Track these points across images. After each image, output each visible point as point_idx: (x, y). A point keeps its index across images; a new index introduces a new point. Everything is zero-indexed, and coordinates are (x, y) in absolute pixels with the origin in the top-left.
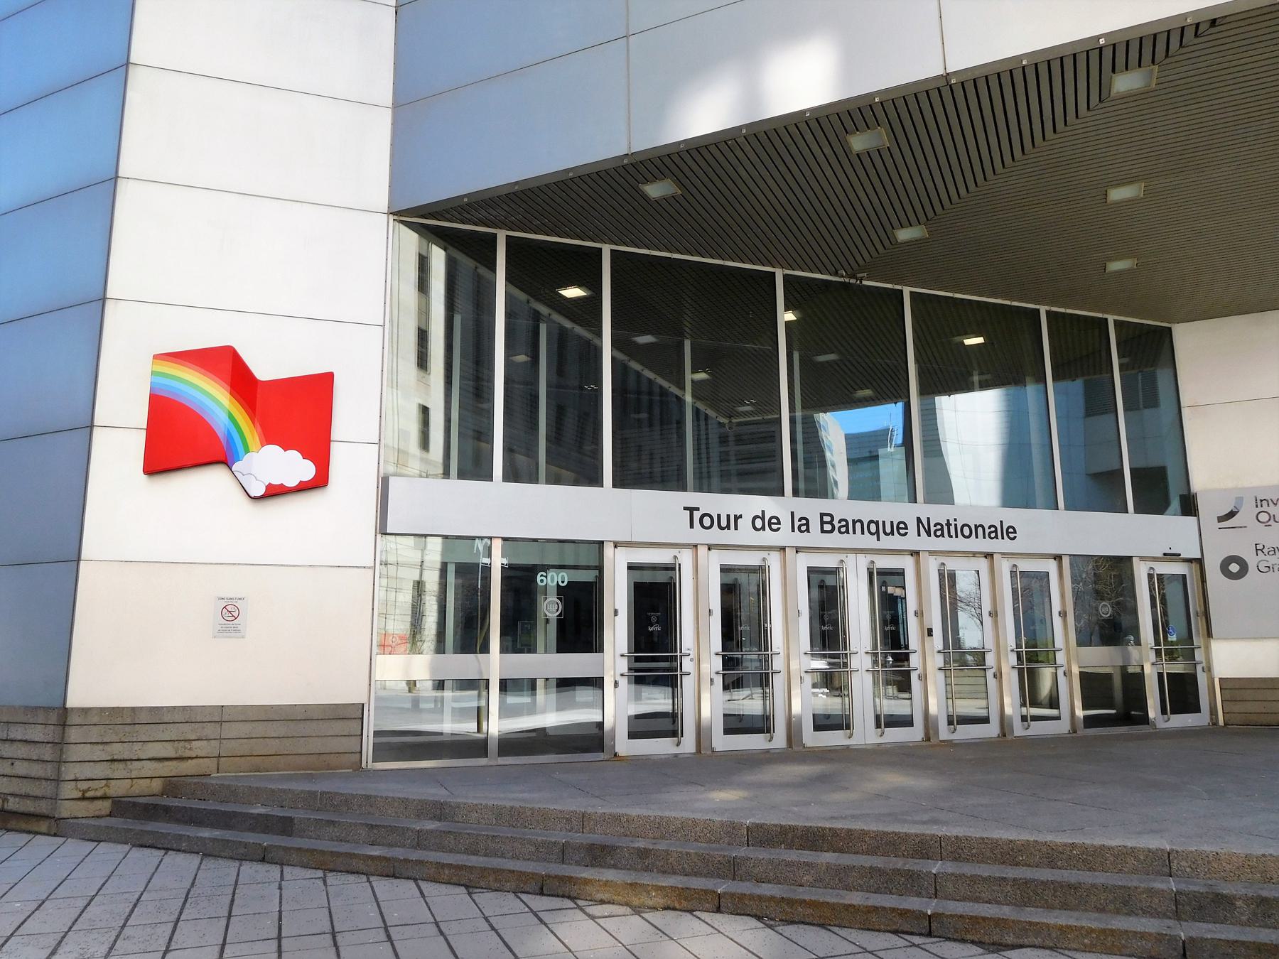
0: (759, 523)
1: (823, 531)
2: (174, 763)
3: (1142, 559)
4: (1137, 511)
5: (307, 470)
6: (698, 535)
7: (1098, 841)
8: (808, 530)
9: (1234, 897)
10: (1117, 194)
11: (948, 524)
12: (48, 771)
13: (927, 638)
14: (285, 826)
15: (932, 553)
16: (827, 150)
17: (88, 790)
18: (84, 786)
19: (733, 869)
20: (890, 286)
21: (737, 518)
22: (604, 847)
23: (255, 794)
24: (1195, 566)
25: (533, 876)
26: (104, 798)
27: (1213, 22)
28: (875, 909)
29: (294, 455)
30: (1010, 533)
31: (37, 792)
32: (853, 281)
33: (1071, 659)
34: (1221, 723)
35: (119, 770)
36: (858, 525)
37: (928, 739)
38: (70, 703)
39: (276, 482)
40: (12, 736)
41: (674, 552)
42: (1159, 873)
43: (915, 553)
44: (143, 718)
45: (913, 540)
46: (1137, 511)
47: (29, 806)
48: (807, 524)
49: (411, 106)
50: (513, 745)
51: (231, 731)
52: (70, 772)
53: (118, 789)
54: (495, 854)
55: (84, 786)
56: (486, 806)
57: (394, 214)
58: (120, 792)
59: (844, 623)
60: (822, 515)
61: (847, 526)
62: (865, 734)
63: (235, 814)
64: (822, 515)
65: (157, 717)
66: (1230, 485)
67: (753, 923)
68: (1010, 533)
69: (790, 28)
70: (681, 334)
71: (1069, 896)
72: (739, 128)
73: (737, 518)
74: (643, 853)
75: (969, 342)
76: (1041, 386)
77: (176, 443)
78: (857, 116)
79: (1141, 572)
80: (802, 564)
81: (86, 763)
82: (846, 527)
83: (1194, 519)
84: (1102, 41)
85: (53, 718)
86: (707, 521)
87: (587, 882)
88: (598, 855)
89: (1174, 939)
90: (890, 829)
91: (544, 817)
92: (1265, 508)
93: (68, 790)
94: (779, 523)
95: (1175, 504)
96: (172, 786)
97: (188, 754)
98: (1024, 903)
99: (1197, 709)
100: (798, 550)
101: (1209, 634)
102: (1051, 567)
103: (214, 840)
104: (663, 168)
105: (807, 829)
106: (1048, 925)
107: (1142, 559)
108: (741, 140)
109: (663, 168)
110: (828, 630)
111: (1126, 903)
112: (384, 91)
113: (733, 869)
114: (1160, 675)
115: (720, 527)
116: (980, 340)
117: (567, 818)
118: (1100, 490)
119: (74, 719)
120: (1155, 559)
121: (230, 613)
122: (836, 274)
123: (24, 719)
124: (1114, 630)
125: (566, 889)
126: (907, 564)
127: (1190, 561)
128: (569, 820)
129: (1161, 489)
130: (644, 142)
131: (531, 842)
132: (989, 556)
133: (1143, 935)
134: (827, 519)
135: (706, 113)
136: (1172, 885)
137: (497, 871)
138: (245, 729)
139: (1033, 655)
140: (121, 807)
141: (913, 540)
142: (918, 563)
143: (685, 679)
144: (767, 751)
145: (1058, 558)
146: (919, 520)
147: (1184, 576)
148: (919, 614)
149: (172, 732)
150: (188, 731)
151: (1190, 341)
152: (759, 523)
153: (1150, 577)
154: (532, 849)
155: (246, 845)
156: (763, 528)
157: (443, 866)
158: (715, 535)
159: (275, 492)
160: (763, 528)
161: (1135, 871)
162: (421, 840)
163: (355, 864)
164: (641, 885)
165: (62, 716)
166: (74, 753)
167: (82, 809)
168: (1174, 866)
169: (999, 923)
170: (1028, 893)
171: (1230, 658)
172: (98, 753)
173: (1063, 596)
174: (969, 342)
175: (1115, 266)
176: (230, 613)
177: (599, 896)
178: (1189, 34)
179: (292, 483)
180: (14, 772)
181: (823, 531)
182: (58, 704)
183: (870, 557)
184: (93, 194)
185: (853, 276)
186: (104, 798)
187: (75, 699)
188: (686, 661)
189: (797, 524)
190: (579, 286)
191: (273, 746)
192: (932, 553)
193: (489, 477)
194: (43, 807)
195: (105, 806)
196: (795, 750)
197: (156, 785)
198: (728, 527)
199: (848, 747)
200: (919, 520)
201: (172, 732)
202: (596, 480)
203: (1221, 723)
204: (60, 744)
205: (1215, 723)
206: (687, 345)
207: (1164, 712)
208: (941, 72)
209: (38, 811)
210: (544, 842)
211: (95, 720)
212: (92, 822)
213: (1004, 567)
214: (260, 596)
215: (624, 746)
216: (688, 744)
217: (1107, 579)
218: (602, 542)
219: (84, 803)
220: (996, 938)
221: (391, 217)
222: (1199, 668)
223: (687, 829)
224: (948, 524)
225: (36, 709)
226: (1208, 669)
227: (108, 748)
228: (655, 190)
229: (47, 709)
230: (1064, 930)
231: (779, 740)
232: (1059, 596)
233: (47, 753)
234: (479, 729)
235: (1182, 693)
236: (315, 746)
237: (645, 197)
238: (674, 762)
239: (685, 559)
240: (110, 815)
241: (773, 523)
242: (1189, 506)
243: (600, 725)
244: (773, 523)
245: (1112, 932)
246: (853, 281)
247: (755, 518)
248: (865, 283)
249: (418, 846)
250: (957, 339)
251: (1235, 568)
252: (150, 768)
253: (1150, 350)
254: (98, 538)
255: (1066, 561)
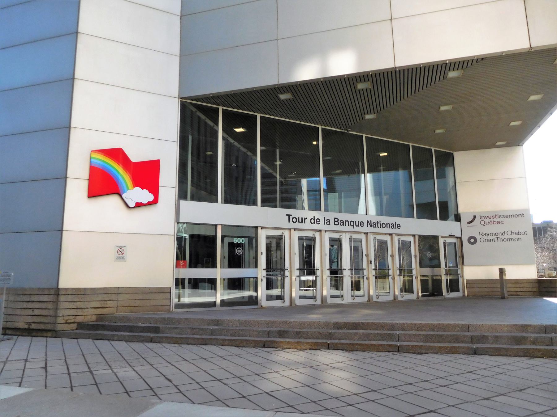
0: (313, 221)
1: (335, 224)
2: (100, 309)
3: (442, 237)
4: (417, 218)
5: (151, 197)
6: (292, 225)
7: (447, 323)
8: (330, 224)
9: (488, 336)
10: (443, 108)
11: (378, 223)
12: (51, 313)
13: (370, 264)
14: (156, 330)
15: (397, 234)
16: (349, 88)
17: (68, 320)
18: (66, 318)
19: (331, 336)
20: (358, 134)
21: (305, 219)
22: (284, 331)
23: (139, 319)
24: (459, 240)
25: (261, 341)
26: (74, 323)
27: (483, 59)
28: (381, 345)
29: (146, 191)
30: (398, 226)
31: (46, 321)
32: (346, 131)
33: (418, 273)
34: (466, 295)
35: (80, 312)
36: (347, 223)
37: (370, 301)
38: (62, 285)
39: (139, 202)
40: (32, 300)
41: (282, 231)
42: (465, 331)
43: (366, 233)
44: (88, 292)
45: (365, 229)
46: (417, 218)
47: (42, 327)
48: (329, 222)
49: (189, 54)
50: (224, 303)
51: (121, 297)
52: (60, 313)
53: (80, 319)
54: (242, 336)
55: (66, 318)
56: (235, 320)
57: (181, 98)
58: (81, 321)
59: (314, 261)
60: (335, 218)
61: (343, 223)
62: (348, 299)
63: (134, 327)
64: (335, 218)
65: (94, 292)
66: (472, 211)
67: (342, 351)
68: (398, 226)
69: (340, 45)
70: (275, 147)
71: (441, 338)
72: (320, 79)
73: (305, 219)
74: (298, 333)
75: (382, 154)
76: (406, 172)
77: (101, 185)
78: (362, 78)
79: (441, 241)
80: (327, 236)
81: (67, 310)
82: (343, 223)
83: (459, 223)
84: (447, 62)
85: (53, 292)
86: (294, 220)
87: (281, 342)
88: (282, 334)
89: (472, 348)
90: (381, 322)
91: (258, 323)
92: (483, 219)
93: (60, 320)
94: (320, 221)
95: (452, 217)
96: (100, 318)
97: (105, 306)
98: (427, 341)
99: (458, 291)
100: (326, 231)
101: (463, 264)
102: (411, 239)
103: (128, 335)
104: (289, 90)
105: (354, 323)
106: (435, 346)
107: (442, 237)
108: (320, 83)
109: (289, 90)
110: (308, 264)
111: (457, 340)
112: (176, 48)
113: (331, 336)
114: (447, 280)
115: (299, 222)
116: (386, 154)
117: (267, 323)
118: (427, 210)
119: (62, 292)
120: (446, 237)
121: (121, 252)
122: (341, 129)
123: (38, 293)
124: (434, 262)
125: (274, 345)
126: (388, 238)
127: (457, 238)
128: (267, 324)
129: (445, 210)
130: (284, 80)
131: (256, 331)
132: (391, 235)
133: (463, 348)
134: (336, 220)
135: (307, 72)
136: (470, 334)
137: (247, 340)
138: (127, 296)
139: (406, 271)
140: (81, 326)
141: (365, 229)
142: (367, 237)
143: (286, 278)
144: (314, 305)
145: (414, 236)
146: (368, 221)
147: (455, 243)
148: (367, 255)
149: (100, 298)
150: (105, 297)
151: (458, 157)
152: (313, 221)
153: (444, 243)
154: (257, 333)
155: (143, 337)
156: (314, 223)
157: (226, 340)
158: (297, 226)
159: (139, 205)
160: (314, 223)
161: (458, 331)
162: (213, 332)
163: (190, 341)
164: (301, 342)
165: (57, 291)
166: (62, 305)
167: (66, 327)
168: (470, 329)
169: (421, 347)
170: (427, 338)
171: (471, 272)
172: (72, 305)
173: (415, 250)
174: (382, 154)
175: (438, 131)
176: (121, 252)
177: (285, 347)
178: (474, 62)
179: (145, 202)
180: (34, 314)
181: (335, 224)
182: (55, 286)
183: (351, 234)
184: (65, 84)
185: (346, 130)
186: (74, 323)
187: (63, 284)
188: (286, 272)
189: (326, 222)
190: (243, 128)
191: (138, 303)
192: (397, 234)
193: (216, 201)
194: (49, 327)
195: (74, 326)
196: (324, 304)
197: (94, 318)
198: (302, 222)
199: (342, 304)
200: (368, 221)
201: (100, 298)
202: (255, 204)
203: (466, 295)
204: (56, 302)
205: (464, 296)
206: (278, 151)
207: (448, 292)
208: (393, 66)
209: (46, 328)
210: (261, 331)
211: (70, 293)
212: (72, 331)
213: (396, 239)
214: (116, 244)
215: (265, 303)
216: (287, 303)
217: (429, 243)
218: (257, 228)
219: (66, 325)
220: (419, 351)
221: (180, 100)
222: (459, 276)
223: (312, 324)
224: (378, 223)
225: (44, 289)
226: (463, 277)
227: (75, 304)
228: (283, 97)
229: (42, 291)
230: (440, 347)
231: (319, 302)
232: (414, 249)
233: (50, 306)
234: (179, 301)
235: (454, 285)
236: (153, 303)
237: (279, 99)
238: (282, 308)
239: (286, 233)
240: (76, 329)
241: (317, 221)
242: (458, 218)
243: (256, 297)
244: (317, 221)
245: (454, 347)
246: (346, 131)
247: (311, 219)
248: (350, 132)
249: (212, 334)
250: (378, 153)
251: (473, 240)
252: (92, 311)
253: (446, 160)
254: (70, 222)
255: (417, 237)
